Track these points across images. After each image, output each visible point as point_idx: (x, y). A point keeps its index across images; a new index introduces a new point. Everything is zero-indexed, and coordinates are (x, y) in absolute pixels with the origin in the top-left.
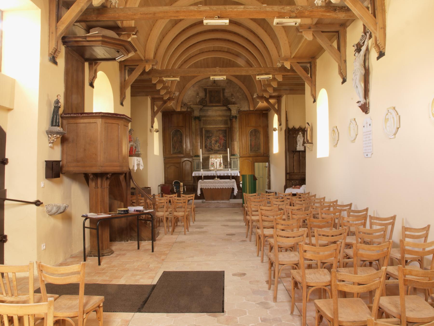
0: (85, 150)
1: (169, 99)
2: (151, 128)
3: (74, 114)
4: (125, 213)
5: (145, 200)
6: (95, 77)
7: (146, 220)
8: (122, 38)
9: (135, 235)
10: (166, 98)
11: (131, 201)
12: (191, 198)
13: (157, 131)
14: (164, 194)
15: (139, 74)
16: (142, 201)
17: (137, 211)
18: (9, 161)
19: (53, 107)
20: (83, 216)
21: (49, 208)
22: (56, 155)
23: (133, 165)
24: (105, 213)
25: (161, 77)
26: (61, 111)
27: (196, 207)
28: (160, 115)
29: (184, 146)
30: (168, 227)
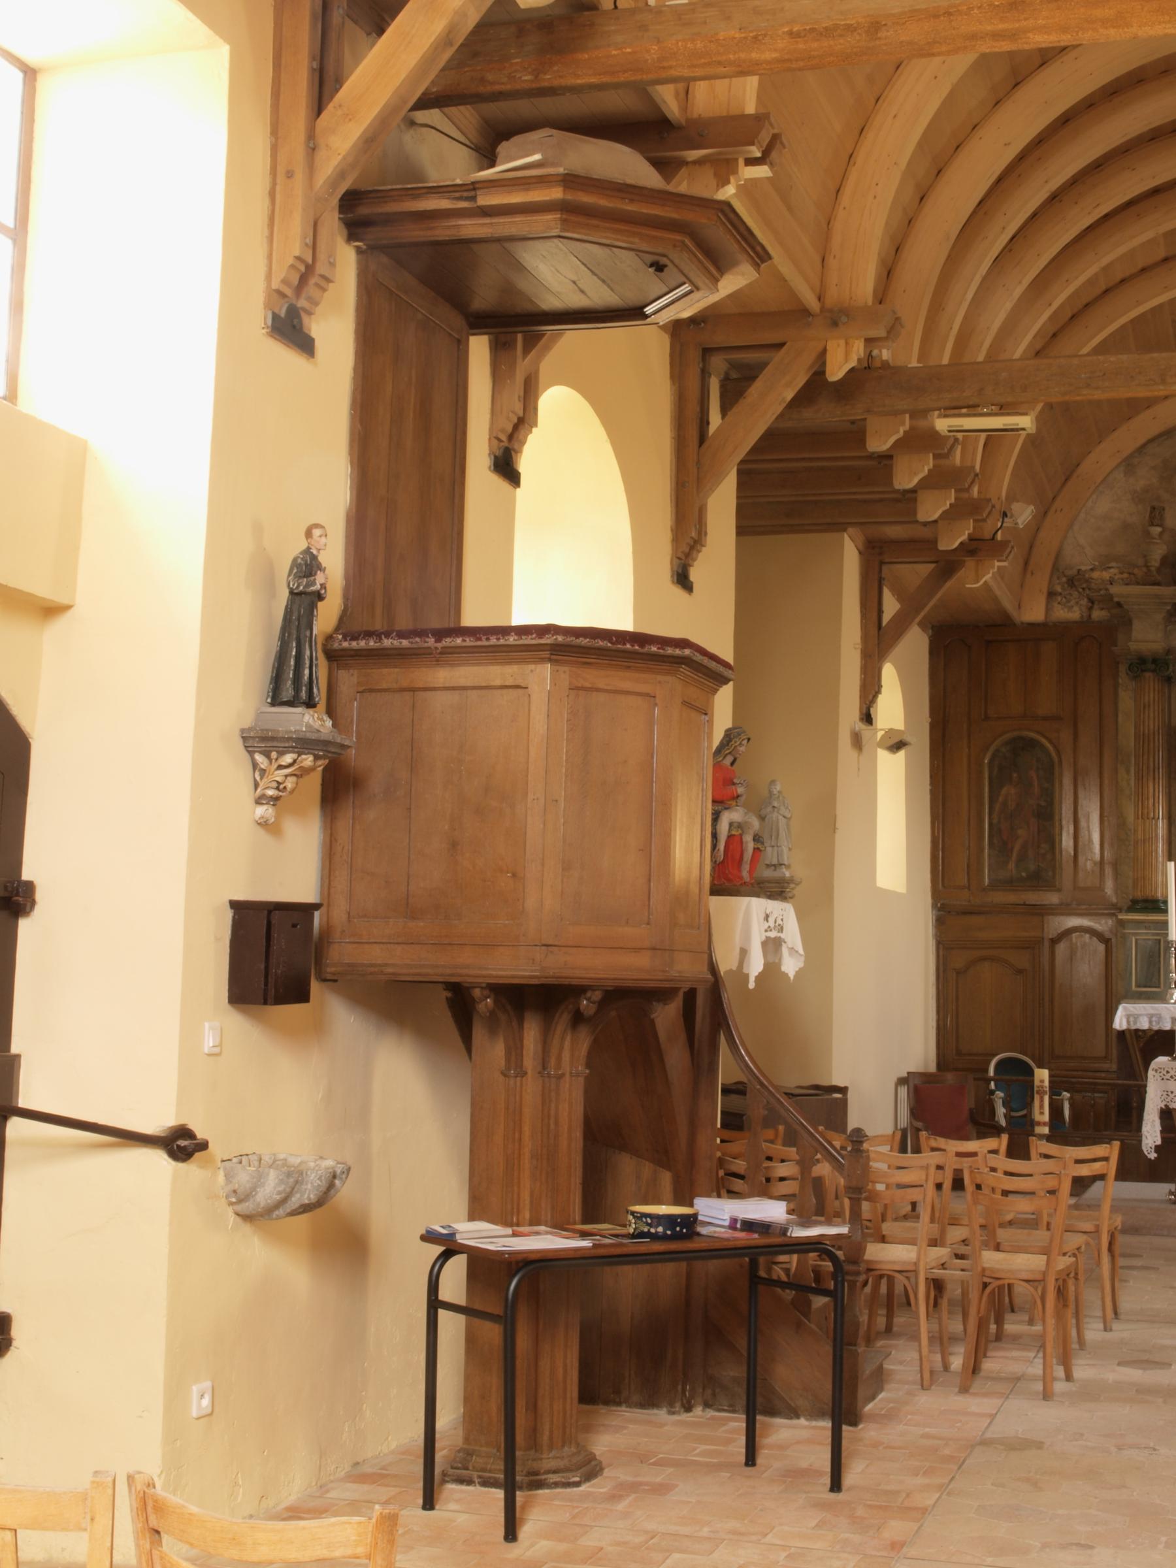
0: (454, 845)
1: (975, 548)
2: (860, 726)
3: (401, 635)
4: (676, 1237)
5: (805, 1164)
6: (524, 421)
7: (803, 1288)
8: (682, 185)
9: (733, 1372)
10: (951, 541)
11: (721, 1162)
12: (1097, 1168)
13: (898, 746)
14: (923, 1134)
15: (789, 395)
16: (782, 1170)
17: (749, 1226)
18: (38, 896)
19: (284, 596)
20: (429, 1237)
21: (243, 1178)
22: (292, 870)
23: (738, 942)
24: (560, 1225)
25: (925, 413)
26: (326, 617)
27: (1130, 1230)
28: (915, 644)
29: (1067, 842)
30: (942, 1341)
